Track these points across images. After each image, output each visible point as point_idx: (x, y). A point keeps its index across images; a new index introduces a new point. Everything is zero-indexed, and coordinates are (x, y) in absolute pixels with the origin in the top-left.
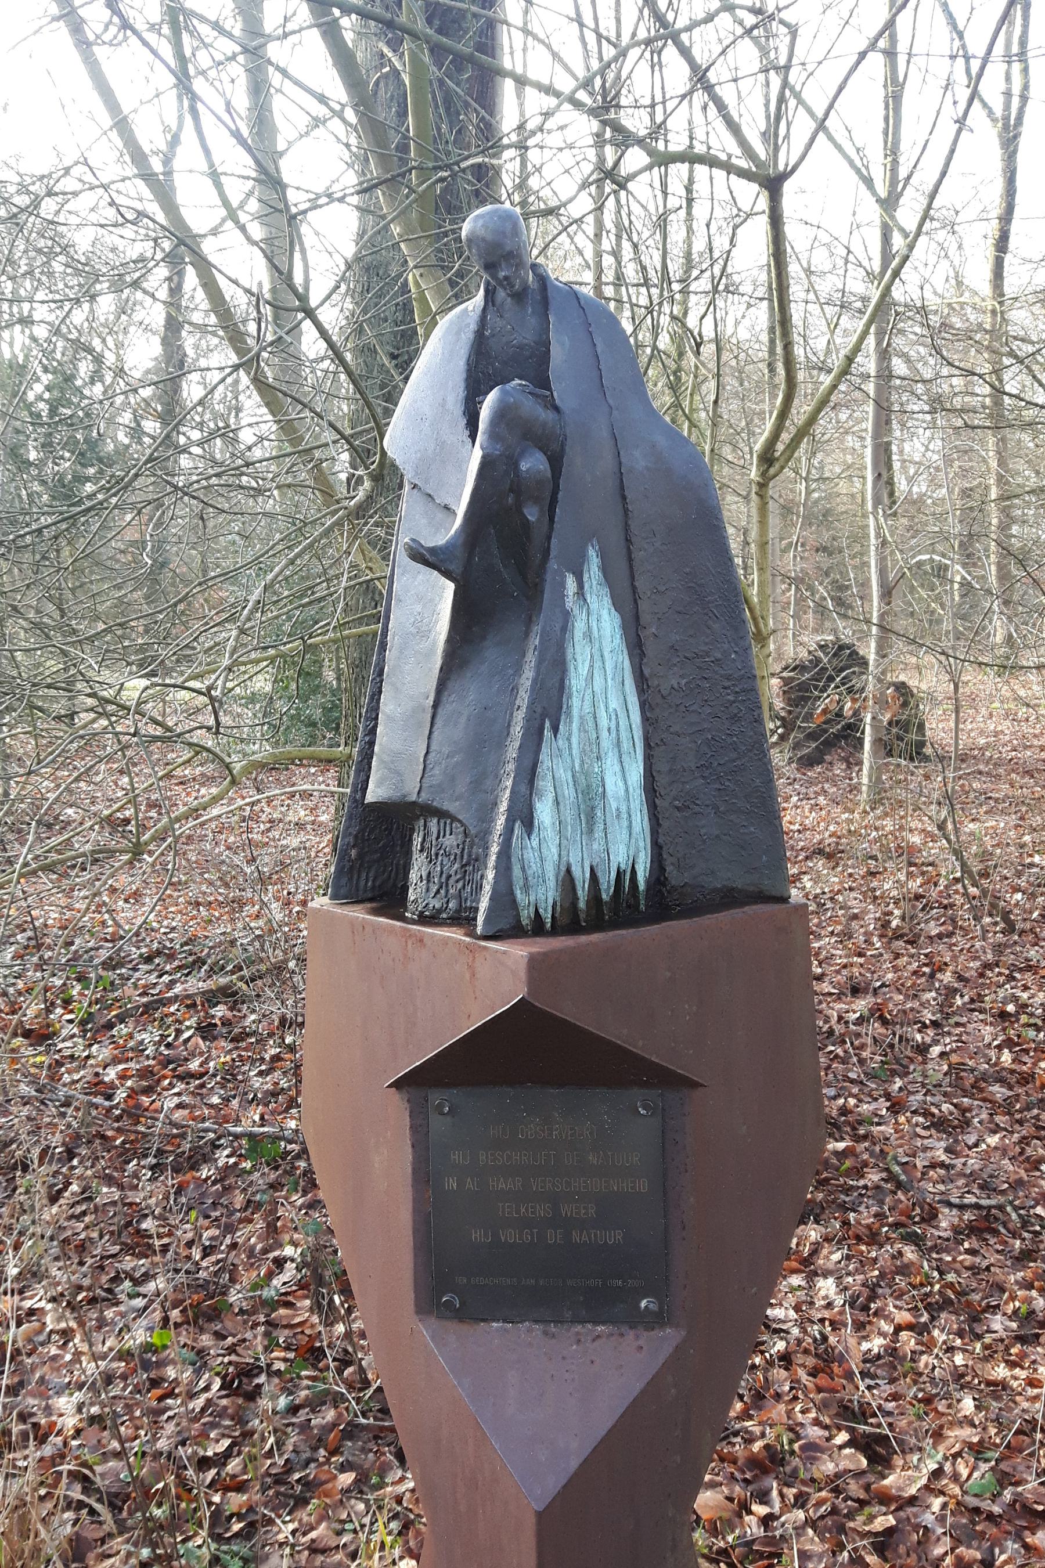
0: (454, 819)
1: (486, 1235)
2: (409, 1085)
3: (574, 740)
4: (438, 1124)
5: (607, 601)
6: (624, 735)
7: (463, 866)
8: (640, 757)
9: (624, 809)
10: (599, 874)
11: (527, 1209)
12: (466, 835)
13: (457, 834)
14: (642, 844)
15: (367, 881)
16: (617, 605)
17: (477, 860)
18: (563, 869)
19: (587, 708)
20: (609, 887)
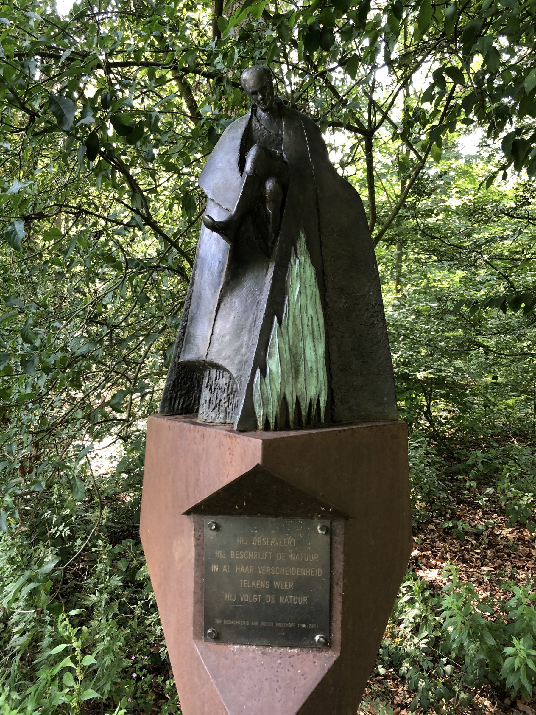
0: (225, 370)
1: (233, 597)
2: (194, 513)
3: (290, 329)
4: (210, 534)
5: (308, 260)
6: (316, 329)
7: (228, 395)
8: (323, 339)
9: (314, 367)
10: (301, 401)
11: (256, 584)
12: (230, 378)
13: (226, 378)
14: (323, 387)
15: (178, 404)
16: (314, 262)
17: (235, 391)
18: (282, 396)
19: (297, 312)
20: (306, 408)
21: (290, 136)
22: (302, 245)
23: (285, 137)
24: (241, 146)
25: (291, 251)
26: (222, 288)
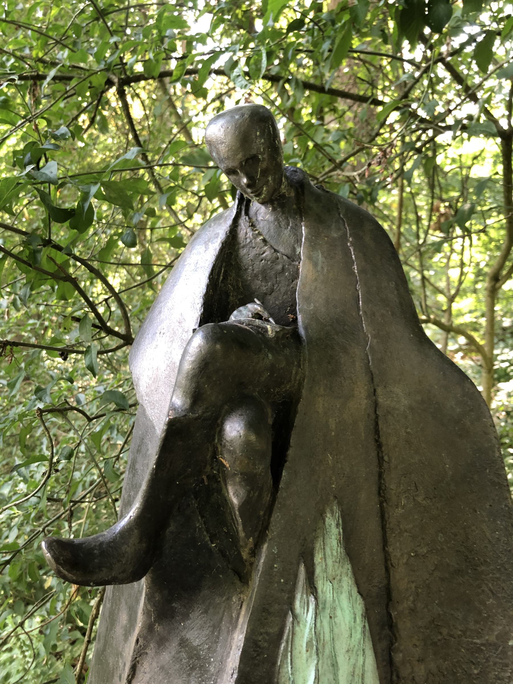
21: (315, 265)
22: (329, 552)
23: (304, 267)
24: (208, 286)
25: (296, 576)
26: (139, 635)
